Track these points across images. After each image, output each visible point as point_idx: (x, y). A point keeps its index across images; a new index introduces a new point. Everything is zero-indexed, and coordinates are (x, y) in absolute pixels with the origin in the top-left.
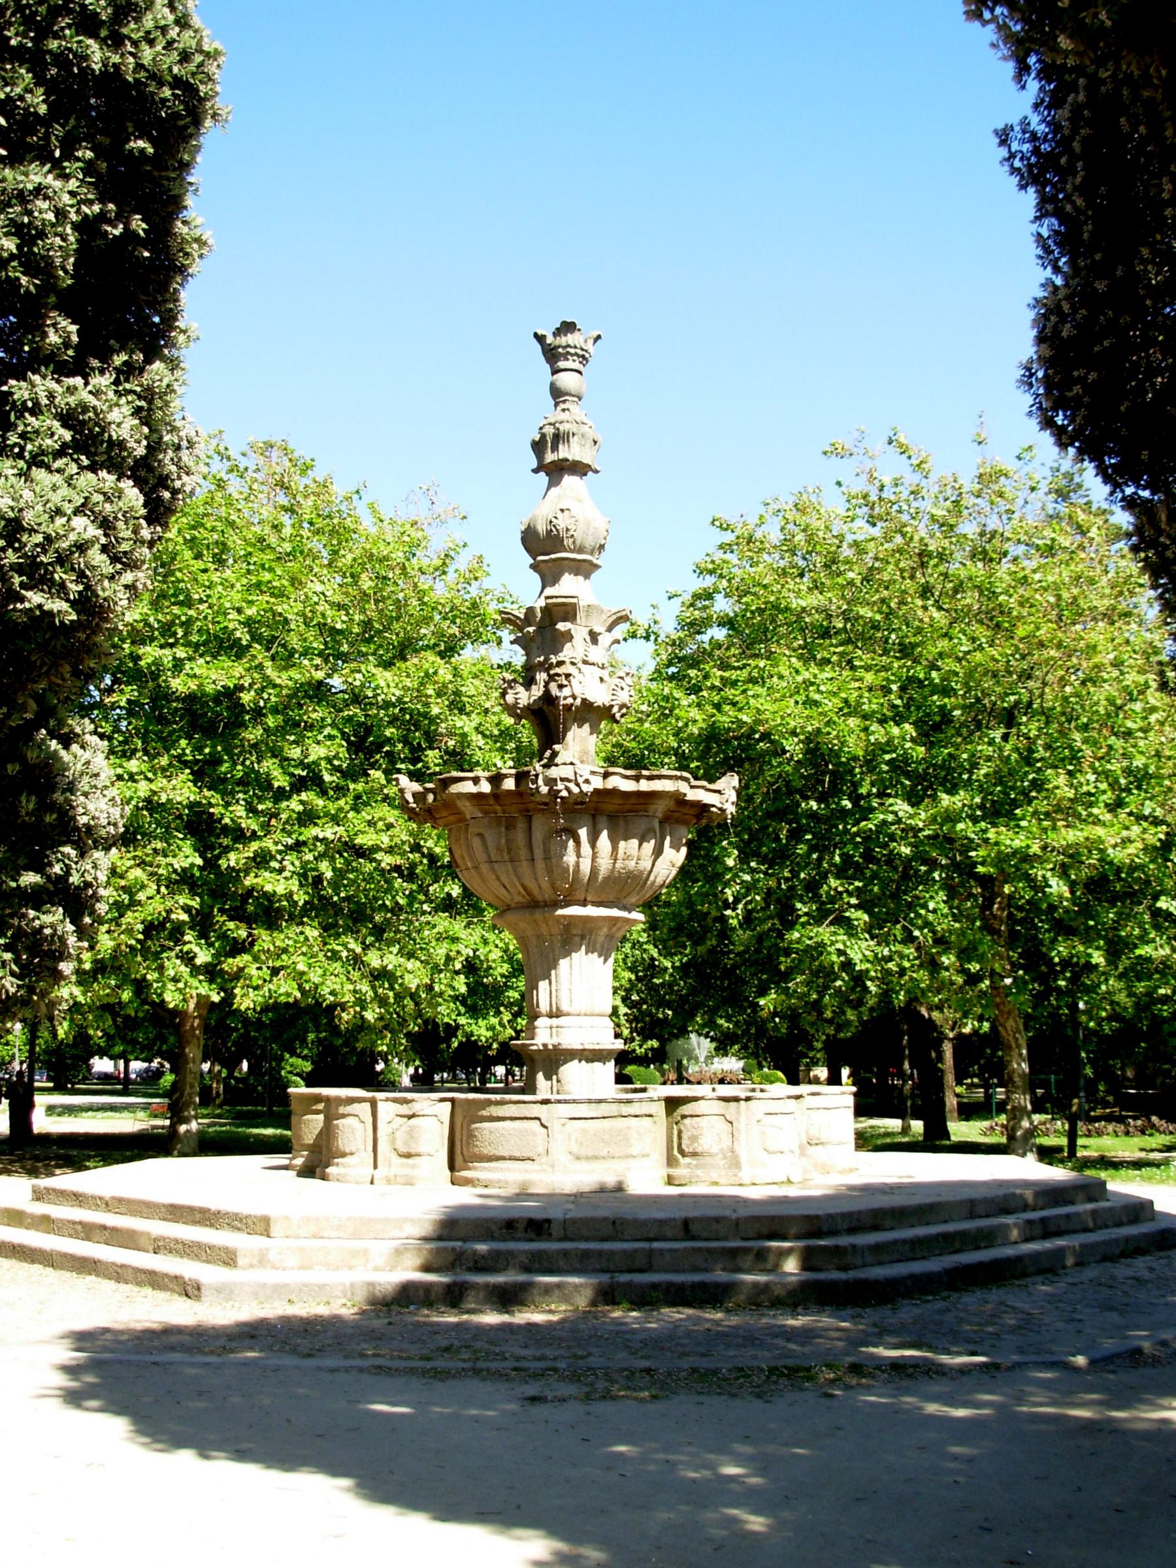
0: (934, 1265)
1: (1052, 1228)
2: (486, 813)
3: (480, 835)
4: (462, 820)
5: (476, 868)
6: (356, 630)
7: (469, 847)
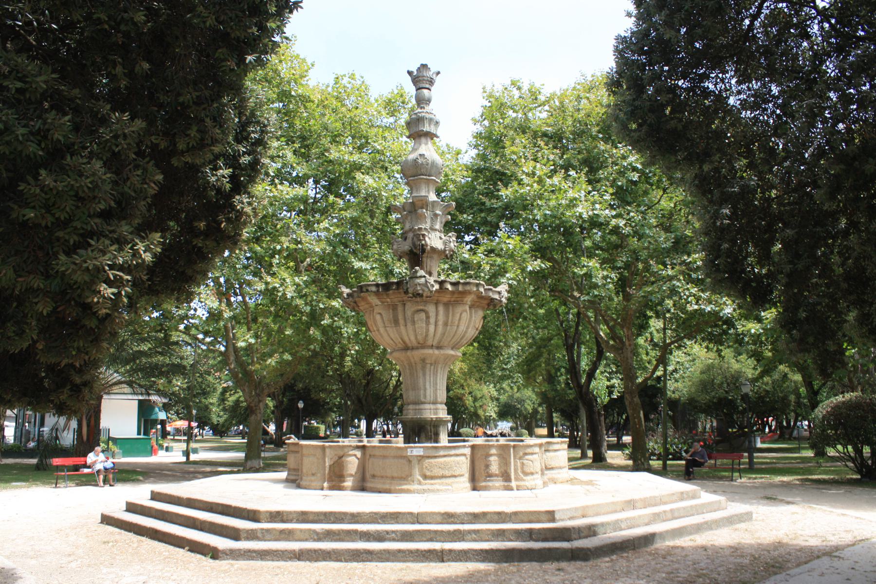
0: (437, 546)
1: (676, 514)
2: (383, 302)
3: (380, 314)
4: (372, 307)
5: (378, 330)
6: (123, 84)
7: (375, 320)
